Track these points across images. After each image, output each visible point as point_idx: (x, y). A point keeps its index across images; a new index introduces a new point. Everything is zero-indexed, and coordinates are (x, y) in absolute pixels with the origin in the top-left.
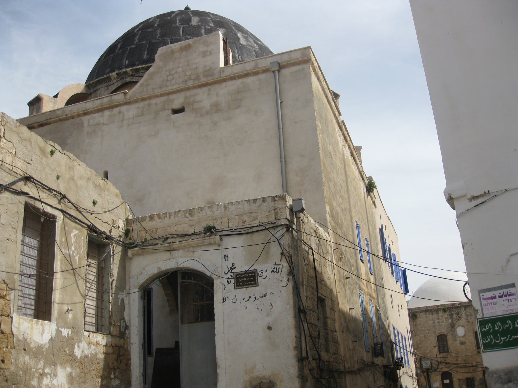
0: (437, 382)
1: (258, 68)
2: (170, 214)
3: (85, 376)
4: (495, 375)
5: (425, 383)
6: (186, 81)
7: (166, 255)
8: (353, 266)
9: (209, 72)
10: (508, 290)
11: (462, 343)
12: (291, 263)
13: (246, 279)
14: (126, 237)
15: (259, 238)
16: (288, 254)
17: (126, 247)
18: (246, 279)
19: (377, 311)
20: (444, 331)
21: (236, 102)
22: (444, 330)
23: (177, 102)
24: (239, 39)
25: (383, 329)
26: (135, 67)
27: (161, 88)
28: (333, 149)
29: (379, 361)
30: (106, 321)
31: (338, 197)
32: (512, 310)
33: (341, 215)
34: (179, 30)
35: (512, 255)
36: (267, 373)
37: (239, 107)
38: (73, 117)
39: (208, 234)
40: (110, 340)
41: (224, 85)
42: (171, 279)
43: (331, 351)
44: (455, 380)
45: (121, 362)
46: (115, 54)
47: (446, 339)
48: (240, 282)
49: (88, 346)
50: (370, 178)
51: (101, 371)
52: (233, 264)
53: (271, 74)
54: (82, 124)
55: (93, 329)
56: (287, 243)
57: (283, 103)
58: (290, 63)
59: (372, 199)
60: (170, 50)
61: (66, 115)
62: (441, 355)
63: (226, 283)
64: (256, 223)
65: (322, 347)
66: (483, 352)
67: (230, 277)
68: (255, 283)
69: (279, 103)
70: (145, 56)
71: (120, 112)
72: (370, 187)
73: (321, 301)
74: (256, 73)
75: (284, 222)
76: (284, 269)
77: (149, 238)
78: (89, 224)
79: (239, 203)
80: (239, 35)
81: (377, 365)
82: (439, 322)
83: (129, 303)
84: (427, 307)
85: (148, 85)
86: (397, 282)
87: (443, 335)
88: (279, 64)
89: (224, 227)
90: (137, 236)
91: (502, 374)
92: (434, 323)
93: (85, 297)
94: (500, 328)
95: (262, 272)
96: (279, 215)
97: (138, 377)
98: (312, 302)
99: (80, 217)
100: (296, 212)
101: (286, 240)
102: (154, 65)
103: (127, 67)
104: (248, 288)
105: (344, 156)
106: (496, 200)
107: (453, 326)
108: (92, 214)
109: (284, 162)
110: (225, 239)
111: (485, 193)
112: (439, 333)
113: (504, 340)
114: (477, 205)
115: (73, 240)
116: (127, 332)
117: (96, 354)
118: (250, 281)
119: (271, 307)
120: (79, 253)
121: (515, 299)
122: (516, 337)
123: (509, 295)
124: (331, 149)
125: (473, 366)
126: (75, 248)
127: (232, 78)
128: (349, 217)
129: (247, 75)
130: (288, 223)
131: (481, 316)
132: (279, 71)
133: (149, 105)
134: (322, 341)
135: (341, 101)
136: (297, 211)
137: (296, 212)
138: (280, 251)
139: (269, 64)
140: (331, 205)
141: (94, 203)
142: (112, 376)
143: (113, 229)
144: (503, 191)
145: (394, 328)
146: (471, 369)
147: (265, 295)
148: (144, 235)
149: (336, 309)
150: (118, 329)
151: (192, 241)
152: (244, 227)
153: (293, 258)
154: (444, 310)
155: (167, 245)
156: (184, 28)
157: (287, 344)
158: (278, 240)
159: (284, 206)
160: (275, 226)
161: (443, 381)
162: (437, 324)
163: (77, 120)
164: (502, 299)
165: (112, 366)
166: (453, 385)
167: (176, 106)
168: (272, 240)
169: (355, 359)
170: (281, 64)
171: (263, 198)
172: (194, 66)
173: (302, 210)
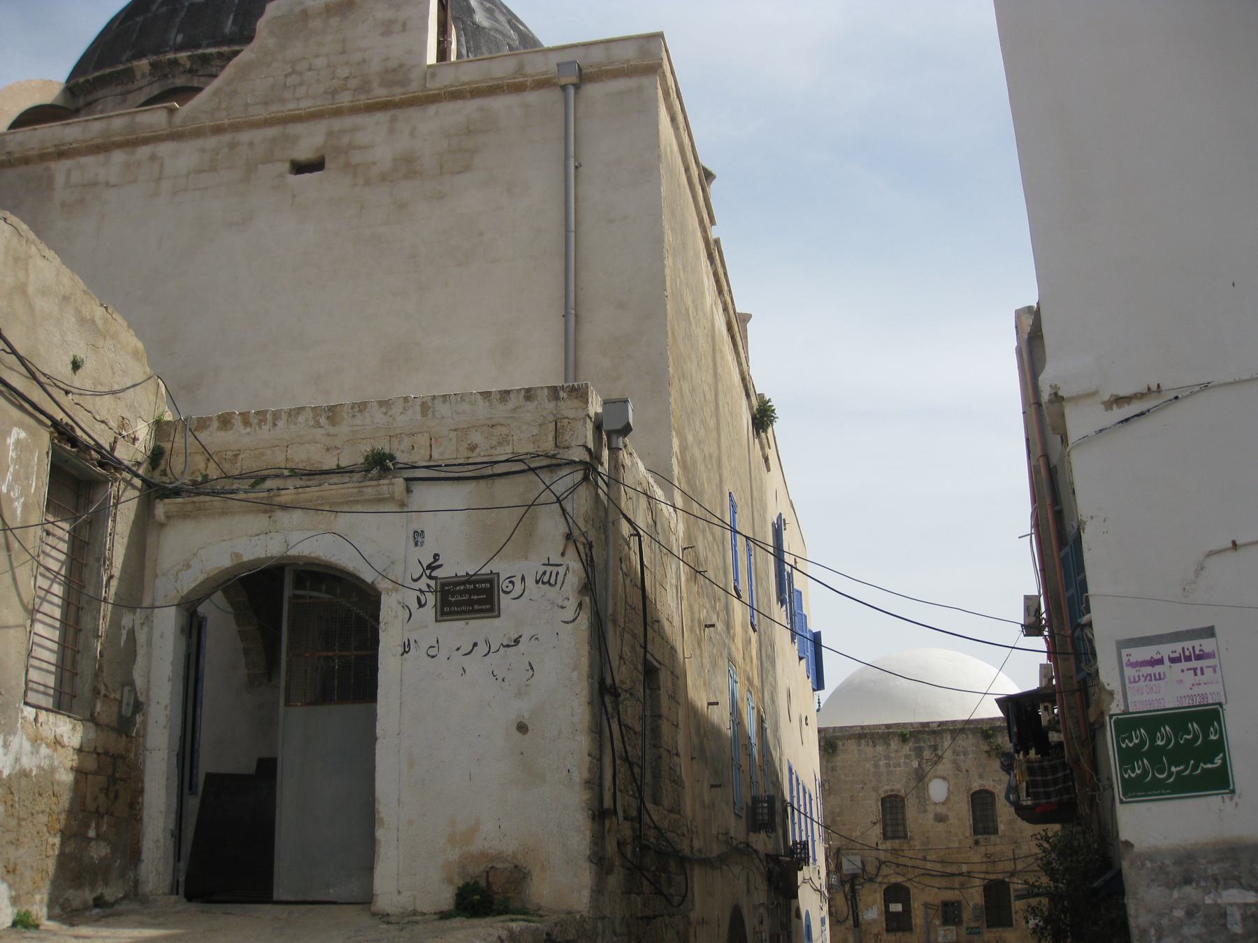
0: (875, 909)
1: (526, 76)
2: (276, 416)
3: (19, 825)
4: (1148, 864)
5: (845, 909)
6: (334, 93)
7: (260, 522)
9: (396, 74)
10: (1196, 643)
11: (940, 819)
12: (588, 563)
13: (468, 598)
14: (153, 469)
15: (509, 492)
16: (583, 540)
17: (153, 492)
18: (468, 598)
19: (761, 721)
20: (899, 786)
22: (898, 785)
23: (308, 142)
25: (769, 765)
26: (200, 51)
27: (266, 103)
29: (761, 842)
30: (84, 686)
31: (698, 423)
32: (1203, 696)
33: (701, 467)
35: (1211, 554)
36: (509, 847)
37: (467, 168)
38: (26, 161)
39: (375, 472)
40: (92, 735)
41: (432, 110)
42: (261, 592)
43: (666, 803)
44: (916, 905)
45: (116, 797)
46: (149, 15)
47: (903, 807)
48: (450, 604)
49: (32, 746)
50: (761, 396)
51: (63, 817)
52: (436, 557)
53: (556, 94)
54: (51, 179)
55: (48, 702)
56: (583, 510)
57: (580, 169)
58: (607, 72)
59: (762, 448)
61: (9, 153)
62: (889, 844)
63: (414, 605)
64: (504, 452)
66: (1121, 802)
67: (425, 588)
68: (492, 610)
69: (571, 166)
70: (228, 27)
71: (153, 158)
72: (762, 417)
73: (650, 673)
74: (518, 88)
75: (578, 455)
76: (569, 576)
77: (213, 473)
78: (59, 415)
79: (462, 397)
81: (755, 851)
82: (888, 765)
83: (149, 642)
84: (862, 727)
86: (801, 659)
87: (896, 796)
88: (580, 70)
89: (419, 457)
90: (179, 468)
91: (1167, 862)
92: (876, 766)
93: (32, 612)
94: (1169, 741)
95: (511, 582)
97: (162, 841)
98: (630, 677)
99: (36, 395)
100: (609, 434)
101: (580, 504)
103: (179, 49)
104: (471, 622)
105: (713, 326)
106: (1178, 406)
107: (920, 778)
108: (67, 393)
109: (572, 315)
110: (418, 489)
113: (1178, 773)
114: (1127, 420)
115: (12, 454)
116: (139, 719)
117: (53, 770)
118: (480, 602)
119: (531, 672)
120: (25, 492)
121: (1214, 668)
122: (1209, 766)
123: (1199, 657)
124: (689, 301)
125: (961, 874)
126: (16, 478)
127: (455, 95)
128: (717, 480)
129: (493, 90)
131: (1122, 708)
132: (577, 87)
133: (233, 146)
134: (648, 778)
135: (714, 188)
136: (612, 430)
138: (562, 528)
139: (553, 68)
141: (76, 366)
142: (92, 833)
143: (120, 441)
145: (790, 769)
146: (957, 880)
147: (517, 641)
148: (202, 466)
150: (116, 709)
151: (332, 489)
152: (471, 461)
153: (594, 551)
154: (904, 738)
155: (261, 495)
157: (565, 773)
158: (559, 501)
159: (581, 414)
160: (555, 465)
161: (887, 907)
162: (883, 769)
164: (1177, 667)
165: (92, 807)
166: (910, 917)
167: (304, 152)
168: (542, 499)
169: (714, 832)
171: (528, 390)
172: (358, 57)
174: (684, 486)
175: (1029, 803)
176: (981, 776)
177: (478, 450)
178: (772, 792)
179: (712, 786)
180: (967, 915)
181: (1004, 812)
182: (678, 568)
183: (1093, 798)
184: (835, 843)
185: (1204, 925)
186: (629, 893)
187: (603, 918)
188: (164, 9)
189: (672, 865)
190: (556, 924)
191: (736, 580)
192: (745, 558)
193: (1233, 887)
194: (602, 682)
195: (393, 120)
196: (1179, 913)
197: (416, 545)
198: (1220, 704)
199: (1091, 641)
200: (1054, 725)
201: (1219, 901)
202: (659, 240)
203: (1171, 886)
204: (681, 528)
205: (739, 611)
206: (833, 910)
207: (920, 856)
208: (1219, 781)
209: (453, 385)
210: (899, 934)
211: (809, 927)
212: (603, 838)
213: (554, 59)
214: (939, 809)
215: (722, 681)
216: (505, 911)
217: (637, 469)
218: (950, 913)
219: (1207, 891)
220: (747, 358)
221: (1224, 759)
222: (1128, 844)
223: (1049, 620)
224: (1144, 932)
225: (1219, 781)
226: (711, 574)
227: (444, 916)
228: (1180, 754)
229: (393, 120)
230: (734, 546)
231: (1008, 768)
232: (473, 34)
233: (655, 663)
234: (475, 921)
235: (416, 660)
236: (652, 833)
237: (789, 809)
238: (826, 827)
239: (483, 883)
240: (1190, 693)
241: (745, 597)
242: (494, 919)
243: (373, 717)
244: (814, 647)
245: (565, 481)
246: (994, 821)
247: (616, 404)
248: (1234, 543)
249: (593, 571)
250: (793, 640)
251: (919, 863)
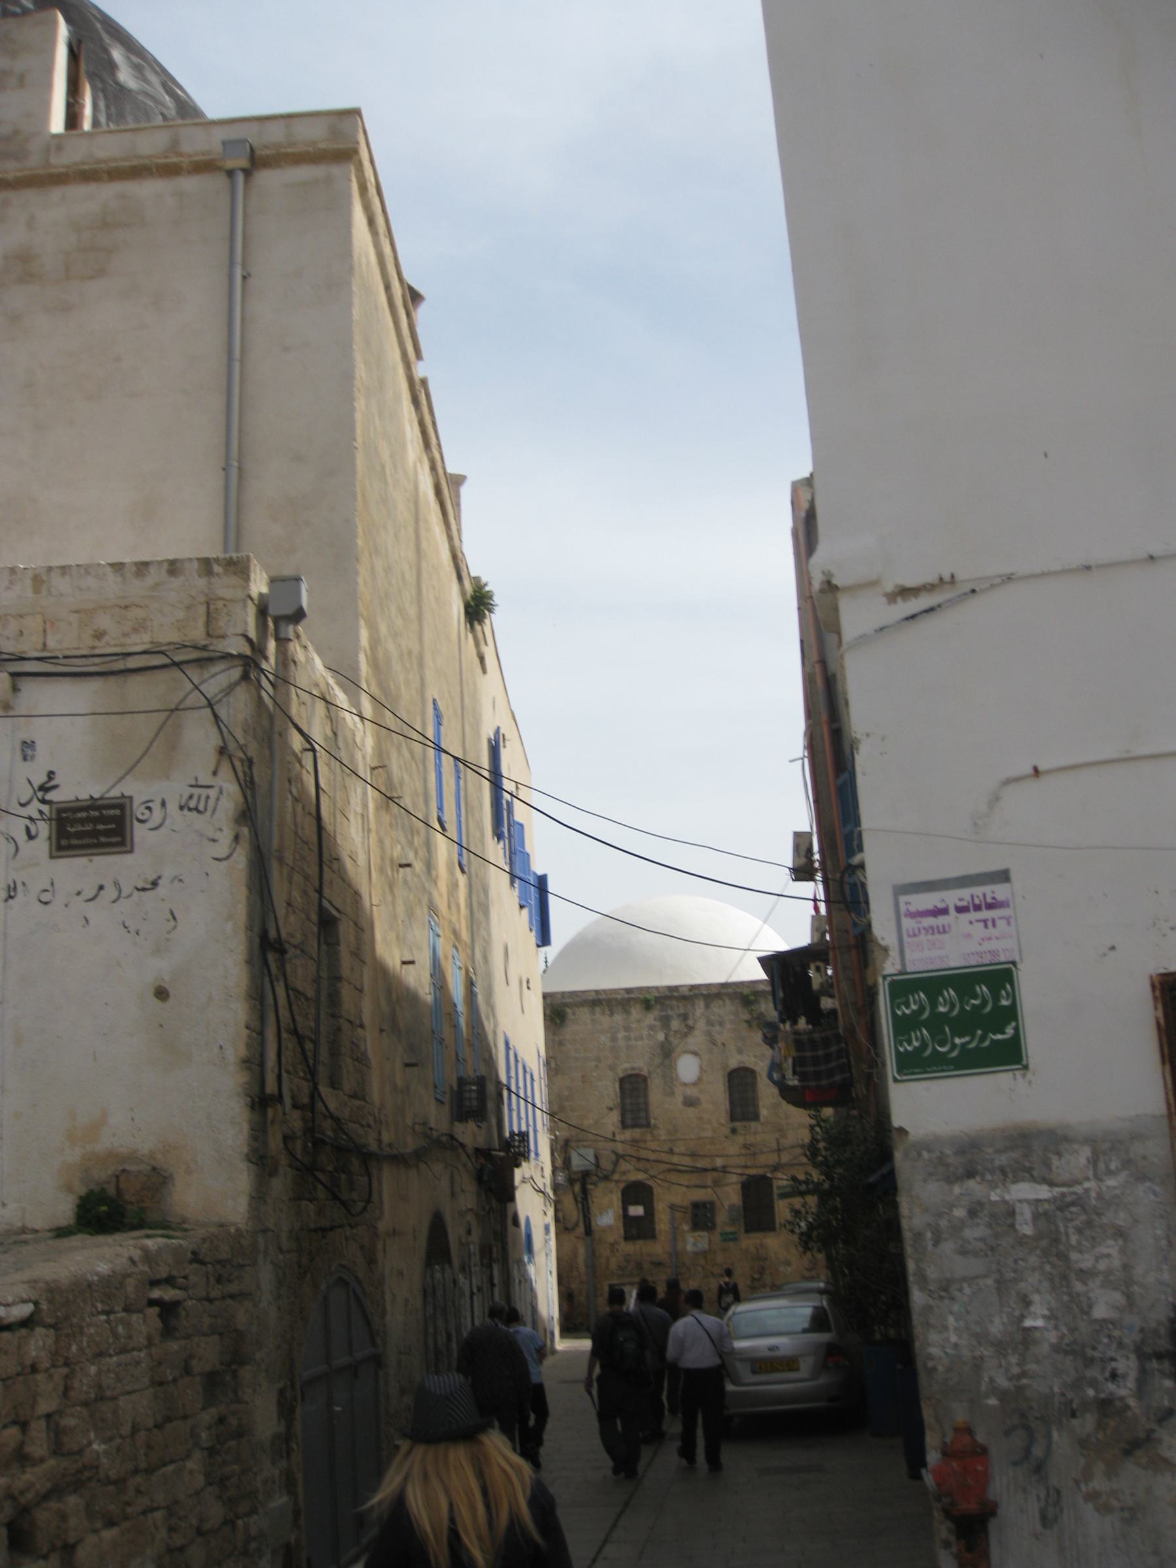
0: (611, 1213)
1: (180, 155)
4: (925, 1155)
8: (418, 833)
11: (690, 1102)
12: (248, 785)
16: (241, 755)
19: (470, 984)
20: (640, 1064)
24: (112, 66)
28: (392, 456)
29: (469, 1134)
32: (994, 953)
33: (397, 666)
35: (1008, 782)
36: (145, 1144)
37: (101, 273)
41: (56, 193)
44: (661, 1207)
48: (69, 836)
50: (476, 581)
52: (51, 775)
53: (220, 181)
58: (287, 155)
59: (477, 644)
62: (628, 1134)
63: (21, 837)
64: (139, 642)
66: (895, 1080)
67: (36, 815)
68: (122, 843)
73: (327, 923)
74: (169, 171)
75: (236, 646)
79: (87, 569)
80: (117, 54)
81: (462, 1145)
82: (628, 1039)
84: (597, 992)
86: (522, 907)
87: (637, 1076)
89: (29, 646)
91: (948, 1152)
92: (614, 1039)
94: (953, 1006)
95: (149, 808)
96: (221, 624)
98: (302, 928)
100: (277, 620)
104: (96, 859)
105: (416, 489)
107: (667, 1053)
109: (235, 470)
110: (27, 686)
111: (941, 579)
112: (626, 1070)
113: (963, 1045)
114: (913, 617)
118: (107, 833)
119: (172, 923)
121: (1008, 920)
122: (999, 1037)
123: (990, 907)
125: (714, 1170)
127: (88, 175)
129: (138, 171)
130: (248, 652)
131: (898, 967)
132: (247, 173)
134: (324, 1054)
135: (422, 314)
136: (281, 616)
137: (277, 620)
138: (215, 741)
139: (217, 147)
140: (373, 628)
144: (999, 580)
145: (507, 1044)
147: (155, 884)
152: (97, 652)
154: (647, 1005)
157: (216, 1050)
158: (210, 705)
159: (240, 594)
160: (206, 659)
162: (621, 1043)
168: (189, 702)
169: (409, 1122)
170: (258, 153)
171: (172, 563)
173: (298, 616)
174: (375, 690)
175: (796, 1083)
176: (740, 1051)
177: (106, 638)
178: (482, 1071)
179: (407, 1065)
180: (721, 1218)
181: (767, 1093)
182: (365, 794)
183: (869, 1076)
184: (563, 1133)
185: (989, 1226)
186: (299, 1199)
187: (265, 1231)
189: (355, 1164)
190: (204, 1240)
191: (440, 809)
192: (452, 782)
193: (1023, 1180)
194: (264, 936)
196: (960, 1213)
197: (25, 759)
198: (1014, 963)
199: (863, 885)
200: (828, 989)
201: (1007, 1197)
202: (348, 376)
203: (950, 1180)
204: (369, 743)
205: (443, 849)
206: (560, 1215)
207: (666, 1148)
208: (1010, 1055)
209: (76, 556)
210: (640, 1242)
212: (264, 1131)
213: (220, 135)
214: (690, 1091)
215: (420, 935)
216: (140, 1224)
217: (312, 666)
218: (701, 1216)
219: (993, 1186)
220: (459, 530)
221: (1017, 1029)
222: (902, 1131)
223: (822, 862)
224: (919, 1236)
225: (1010, 1055)
226: (407, 802)
227: (61, 1233)
228: (965, 1023)
230: (438, 766)
231: (771, 1041)
232: (115, 99)
233: (335, 912)
234: (101, 1239)
236: (328, 1124)
237: (505, 1093)
238: (552, 1115)
239: (111, 1191)
240: (980, 949)
241: (452, 831)
242: (125, 1235)
244: (538, 895)
245: (218, 679)
246: (756, 1106)
247: (285, 583)
248: (1036, 770)
249: (254, 797)
250: (512, 883)
251: (664, 1157)
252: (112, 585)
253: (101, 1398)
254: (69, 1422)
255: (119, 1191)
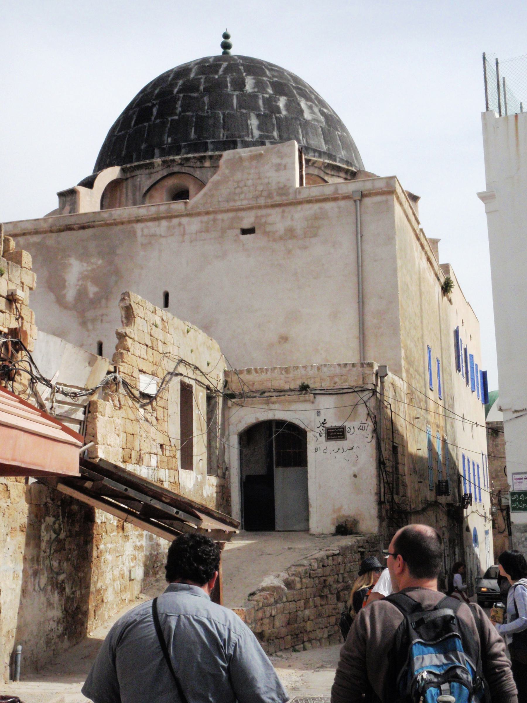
1: (339, 194)
2: (267, 370)
6: (257, 198)
9: (283, 190)
12: (375, 423)
13: (336, 434)
15: (348, 399)
18: (336, 434)
19: (444, 442)
21: (312, 229)
24: (302, 111)
25: (450, 461)
29: (443, 499)
30: (214, 465)
34: (232, 100)
37: (315, 235)
38: (122, 223)
41: (299, 208)
46: (151, 123)
48: (330, 436)
52: (325, 420)
54: (134, 233)
58: (373, 193)
60: (237, 156)
61: (114, 220)
63: (318, 435)
64: (346, 385)
65: (395, 492)
68: (344, 438)
69: (359, 235)
71: (180, 224)
73: (395, 449)
74: (335, 199)
75: (371, 387)
77: (246, 389)
79: (331, 365)
80: (303, 104)
81: (440, 504)
85: (212, 196)
86: (473, 392)
88: (362, 192)
89: (317, 386)
90: (235, 387)
100: (380, 377)
101: (372, 403)
102: (219, 172)
110: (318, 397)
114: (517, 417)
118: (340, 435)
127: (309, 202)
129: (325, 200)
133: (215, 220)
134: (395, 486)
136: (381, 375)
147: (352, 448)
149: (406, 454)
156: (237, 96)
158: (365, 403)
159: (371, 372)
163: (129, 227)
167: (246, 225)
169: (420, 500)
171: (353, 364)
172: (266, 180)
179: (419, 482)
188: (158, 121)
189: (403, 516)
194: (380, 460)
195: (283, 212)
196: (523, 539)
211: (476, 536)
222: (512, 522)
224: (515, 543)
229: (283, 212)
235: (319, 453)
239: (344, 525)
243: (306, 472)
245: (366, 395)
252: (338, 370)
253: (350, 572)
254: (345, 575)
255: (346, 525)
